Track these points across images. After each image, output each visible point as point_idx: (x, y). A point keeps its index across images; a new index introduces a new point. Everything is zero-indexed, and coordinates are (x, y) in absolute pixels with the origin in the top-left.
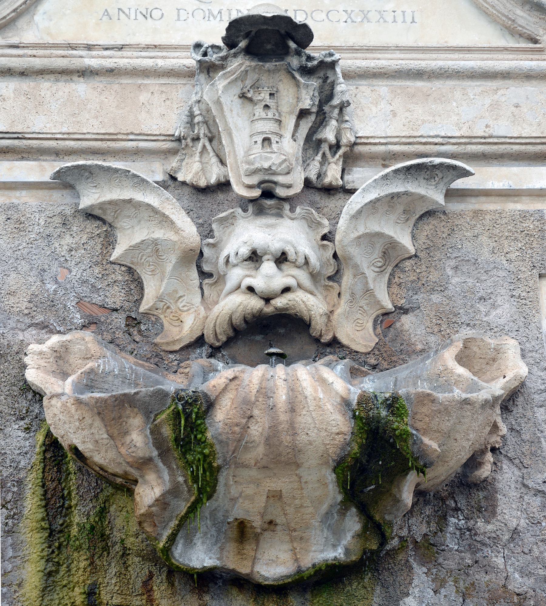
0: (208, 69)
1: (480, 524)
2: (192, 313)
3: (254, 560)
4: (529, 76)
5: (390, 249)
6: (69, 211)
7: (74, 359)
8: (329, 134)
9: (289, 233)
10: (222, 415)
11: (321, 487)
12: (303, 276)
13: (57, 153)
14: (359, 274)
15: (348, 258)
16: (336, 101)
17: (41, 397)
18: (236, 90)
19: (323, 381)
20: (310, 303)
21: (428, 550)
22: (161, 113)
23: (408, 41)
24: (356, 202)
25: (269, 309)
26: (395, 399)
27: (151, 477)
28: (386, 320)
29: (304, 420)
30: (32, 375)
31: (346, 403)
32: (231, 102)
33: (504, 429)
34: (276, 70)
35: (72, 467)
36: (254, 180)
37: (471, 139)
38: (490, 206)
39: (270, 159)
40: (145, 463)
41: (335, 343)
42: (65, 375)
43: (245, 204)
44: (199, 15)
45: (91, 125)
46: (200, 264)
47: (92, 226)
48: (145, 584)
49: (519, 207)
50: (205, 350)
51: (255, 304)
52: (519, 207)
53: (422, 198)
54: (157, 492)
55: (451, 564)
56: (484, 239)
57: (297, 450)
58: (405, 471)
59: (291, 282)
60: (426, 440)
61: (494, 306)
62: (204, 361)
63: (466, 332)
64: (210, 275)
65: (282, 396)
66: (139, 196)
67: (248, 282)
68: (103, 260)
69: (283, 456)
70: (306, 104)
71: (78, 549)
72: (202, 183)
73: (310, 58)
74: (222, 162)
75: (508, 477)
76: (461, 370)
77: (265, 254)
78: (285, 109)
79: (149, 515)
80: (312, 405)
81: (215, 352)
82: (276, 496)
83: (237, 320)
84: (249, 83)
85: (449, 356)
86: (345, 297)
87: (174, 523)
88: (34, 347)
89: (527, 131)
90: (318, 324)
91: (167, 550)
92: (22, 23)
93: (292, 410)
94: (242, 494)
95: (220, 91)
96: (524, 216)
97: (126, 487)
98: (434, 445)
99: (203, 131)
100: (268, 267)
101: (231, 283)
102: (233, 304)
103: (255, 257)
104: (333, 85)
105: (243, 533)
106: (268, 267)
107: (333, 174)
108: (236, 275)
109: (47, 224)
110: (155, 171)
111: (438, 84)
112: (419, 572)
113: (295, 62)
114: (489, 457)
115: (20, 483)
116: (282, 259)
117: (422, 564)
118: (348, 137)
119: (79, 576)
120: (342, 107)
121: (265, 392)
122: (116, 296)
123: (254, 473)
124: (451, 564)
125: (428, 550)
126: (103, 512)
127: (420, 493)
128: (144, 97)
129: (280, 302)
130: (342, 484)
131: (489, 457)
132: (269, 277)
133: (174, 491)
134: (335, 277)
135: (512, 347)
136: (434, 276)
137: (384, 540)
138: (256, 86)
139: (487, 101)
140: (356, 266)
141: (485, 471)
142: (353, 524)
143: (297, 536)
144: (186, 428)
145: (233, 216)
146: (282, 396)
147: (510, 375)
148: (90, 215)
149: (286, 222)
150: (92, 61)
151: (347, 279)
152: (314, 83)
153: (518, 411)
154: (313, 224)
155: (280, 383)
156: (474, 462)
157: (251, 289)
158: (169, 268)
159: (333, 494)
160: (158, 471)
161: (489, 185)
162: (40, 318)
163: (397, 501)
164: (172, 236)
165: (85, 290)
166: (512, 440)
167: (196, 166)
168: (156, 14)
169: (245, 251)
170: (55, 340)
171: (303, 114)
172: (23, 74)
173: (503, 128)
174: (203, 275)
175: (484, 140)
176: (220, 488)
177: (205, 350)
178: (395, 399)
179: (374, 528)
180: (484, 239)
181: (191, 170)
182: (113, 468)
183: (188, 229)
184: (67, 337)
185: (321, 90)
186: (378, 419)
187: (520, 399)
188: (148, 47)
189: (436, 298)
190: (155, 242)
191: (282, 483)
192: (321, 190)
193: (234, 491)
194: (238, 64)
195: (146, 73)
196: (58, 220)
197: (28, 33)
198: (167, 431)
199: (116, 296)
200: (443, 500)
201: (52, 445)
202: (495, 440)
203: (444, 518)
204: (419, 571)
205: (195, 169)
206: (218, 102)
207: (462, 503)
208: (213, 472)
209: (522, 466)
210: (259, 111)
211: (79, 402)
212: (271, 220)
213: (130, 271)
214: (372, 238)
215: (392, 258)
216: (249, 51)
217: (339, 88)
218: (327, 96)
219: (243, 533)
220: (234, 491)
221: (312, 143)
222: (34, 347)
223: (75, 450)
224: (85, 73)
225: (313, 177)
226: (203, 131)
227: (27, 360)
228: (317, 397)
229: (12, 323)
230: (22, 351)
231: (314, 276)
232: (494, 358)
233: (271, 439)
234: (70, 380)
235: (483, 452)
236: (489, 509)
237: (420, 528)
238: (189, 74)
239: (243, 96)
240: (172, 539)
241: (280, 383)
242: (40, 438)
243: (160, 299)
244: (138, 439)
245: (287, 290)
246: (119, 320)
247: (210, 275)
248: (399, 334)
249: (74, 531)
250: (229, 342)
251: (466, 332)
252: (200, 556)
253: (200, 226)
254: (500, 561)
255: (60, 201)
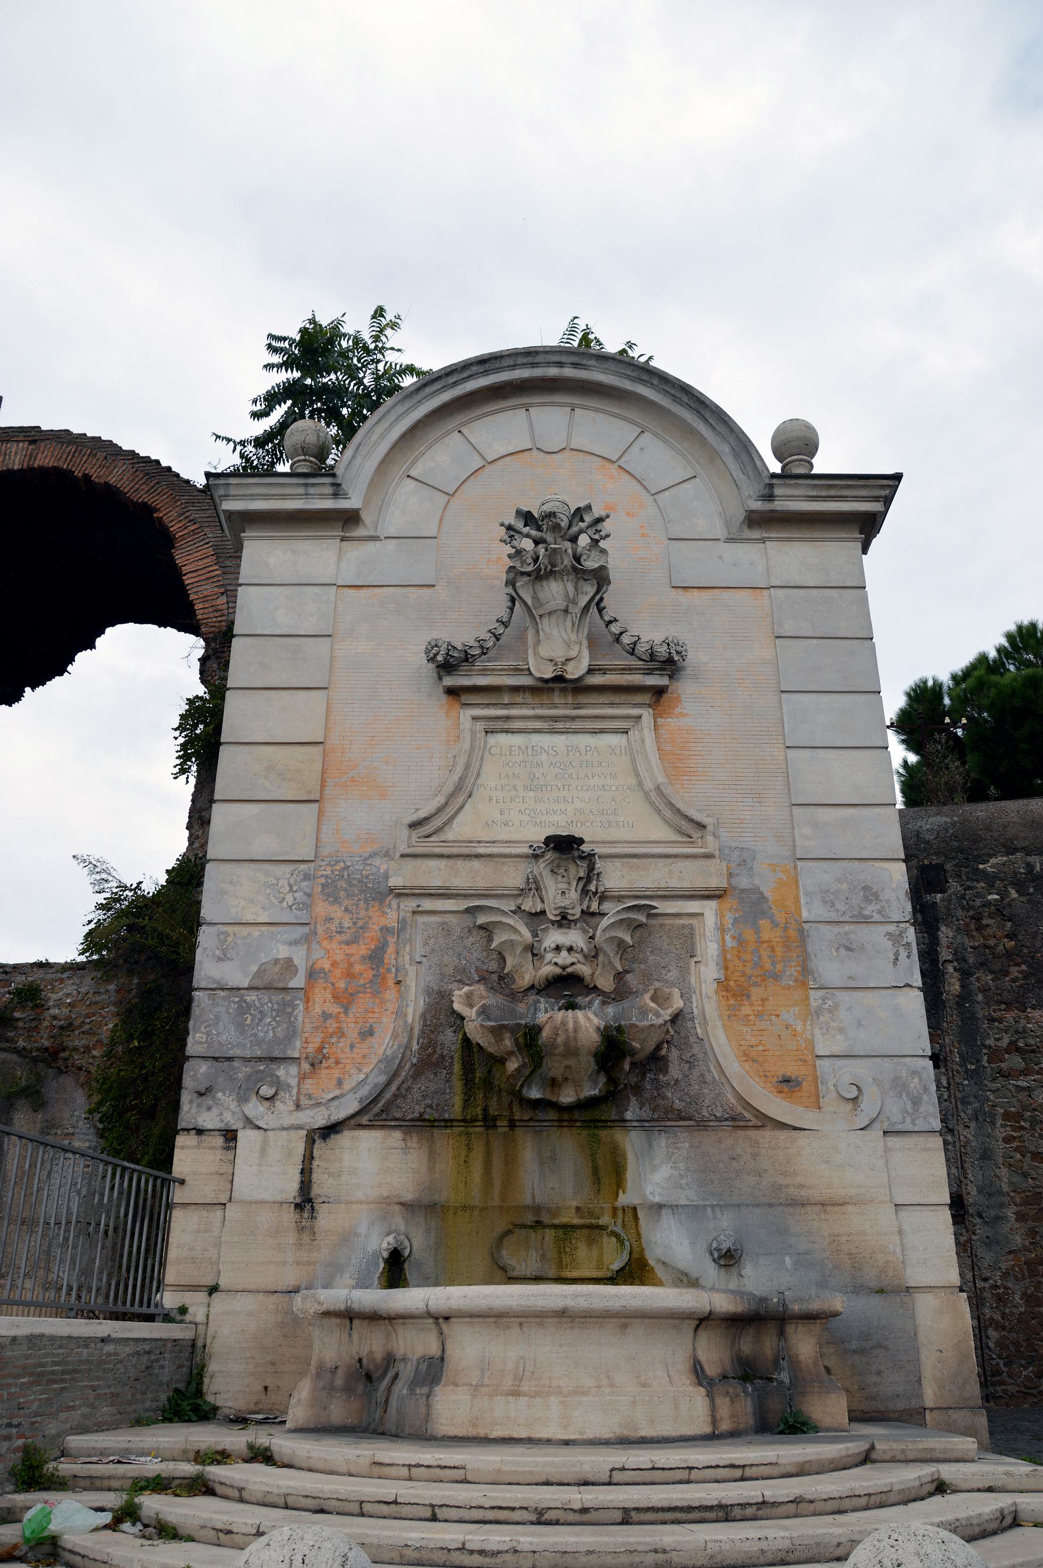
0: (536, 857)
1: (661, 1077)
2: (528, 974)
3: (559, 1095)
4: (687, 856)
5: (621, 943)
6: (471, 925)
7: (476, 999)
8: (592, 888)
9: (574, 937)
10: (545, 1034)
11: (588, 1064)
12: (580, 957)
13: (465, 896)
14: (606, 955)
15: (601, 949)
16: (595, 872)
17: (464, 1018)
18: (549, 868)
19: (589, 1019)
20: (584, 969)
21: (637, 1089)
22: (514, 877)
23: (630, 837)
24: (605, 922)
25: (564, 973)
26: (620, 1026)
27: (513, 1059)
28: (619, 976)
29: (581, 1035)
30: (457, 1006)
31: (598, 1028)
32: (546, 874)
33: (672, 1032)
34: (567, 859)
35: (475, 1050)
36: (558, 912)
37: (659, 889)
38: (668, 921)
39: (565, 903)
40: (511, 1053)
41: (595, 987)
42: (471, 1006)
43: (553, 923)
44: (531, 824)
45: (481, 883)
46: (533, 951)
47: (482, 933)
48: (510, 1105)
49: (681, 922)
50: (535, 991)
51: (558, 970)
52: (681, 922)
53: (635, 920)
54: (516, 1065)
55: (647, 1096)
56: (665, 938)
57: (577, 1049)
58: (625, 1057)
59: (575, 960)
60: (634, 1044)
61: (669, 971)
62: (534, 997)
63: (657, 984)
64: (537, 955)
65: (571, 1025)
66: (504, 920)
67: (555, 960)
68: (487, 949)
69: (571, 1050)
70: (582, 874)
71: (479, 1089)
72: (533, 911)
73: (583, 852)
74: (543, 902)
75: (674, 1054)
76: (652, 1004)
77: (563, 947)
78: (571, 877)
79: (512, 1075)
80: (584, 1029)
81: (539, 992)
82: (569, 1067)
83: (550, 977)
84: (555, 864)
85: (647, 997)
86: (600, 966)
87: (523, 1079)
88: (456, 992)
89: (686, 885)
90: (588, 979)
91: (520, 1091)
92: (446, 828)
93: (575, 1031)
94: (554, 1067)
95: (541, 868)
96: (684, 926)
97: (502, 1061)
98: (638, 1045)
99: (534, 887)
100: (564, 953)
101: (546, 961)
102: (547, 970)
103: (558, 949)
104: (594, 864)
105: (554, 1084)
106: (564, 953)
107: (594, 907)
108: (549, 956)
109: (461, 932)
110: (508, 906)
111: (644, 860)
112: (633, 1100)
113: (576, 853)
114: (665, 1045)
115: (452, 1057)
116: (570, 949)
117: (634, 1096)
118: (601, 889)
119: (479, 1102)
120: (598, 874)
121: (564, 1023)
122: (493, 966)
123: (559, 1058)
124: (647, 1096)
125: (637, 1089)
126: (490, 1072)
127: (632, 1064)
128: (505, 868)
129: (569, 970)
130: (597, 1063)
131: (665, 1045)
132: (565, 958)
133: (524, 1065)
134: (596, 956)
135: (676, 993)
136: (641, 956)
137: (616, 1086)
138: (558, 866)
139: (667, 870)
140: (605, 952)
141: (664, 1052)
142: (603, 1079)
143: (578, 1085)
144: (529, 1039)
145: (547, 928)
146: (571, 1025)
147: (675, 1007)
148: (481, 927)
149: (573, 931)
150: (481, 850)
151: (601, 958)
152: (584, 864)
153: (679, 1023)
154: (585, 931)
155: (570, 1019)
156: (658, 1047)
157: (556, 964)
158: (518, 953)
159: (593, 1066)
160: (516, 1056)
161: (667, 911)
162: (459, 977)
163: (622, 1069)
164: (518, 938)
165: (479, 964)
166: (676, 1037)
167: (530, 903)
168: (510, 823)
169: (553, 946)
170: (466, 988)
171: (580, 879)
172: (449, 857)
173: (674, 883)
174: (534, 955)
175: (665, 889)
176: (544, 1064)
177: (535, 991)
178: (620, 1026)
179: (612, 1080)
180: (665, 938)
181: (528, 905)
182: (496, 1054)
183: (527, 935)
184: (472, 988)
185: (588, 866)
186: (612, 1036)
187: (680, 1017)
188: (506, 842)
189: (642, 966)
190: (512, 941)
191: (571, 1062)
192: (587, 914)
193: (550, 1065)
194: (550, 855)
195: (506, 856)
196: (466, 930)
197: (450, 834)
198: (521, 1040)
199: (493, 966)
200: (644, 1066)
201: (466, 1041)
202: (668, 1037)
203: (645, 1074)
204: (633, 1099)
205: (529, 904)
206: (540, 874)
207: (653, 1067)
208: (541, 1058)
209: (680, 1049)
210: (560, 878)
211: (482, 1026)
212: (566, 930)
213: (500, 953)
214: (612, 939)
215: (621, 946)
216: (554, 848)
217: (597, 866)
218: (591, 868)
219: (554, 1084)
220: (550, 1065)
221: (585, 892)
222: (456, 992)
223: (479, 1045)
224: (478, 856)
225: (585, 909)
226: (534, 887)
227: (453, 998)
228: (587, 1023)
229: (446, 980)
230: (451, 994)
231: (585, 957)
232: (668, 998)
233: (566, 1044)
234: (474, 1009)
235: (662, 1043)
236: (665, 1070)
237: (633, 1079)
238: (527, 856)
239: (552, 871)
240: (522, 1086)
241: (570, 1019)
242: (461, 1036)
243: (514, 967)
244: (508, 1043)
245: (573, 964)
246: (495, 977)
247: (537, 955)
248: (625, 983)
249: (477, 1080)
250: (546, 987)
251: (657, 984)
252: (535, 1094)
253: (531, 931)
254: (670, 1094)
255: (467, 920)
